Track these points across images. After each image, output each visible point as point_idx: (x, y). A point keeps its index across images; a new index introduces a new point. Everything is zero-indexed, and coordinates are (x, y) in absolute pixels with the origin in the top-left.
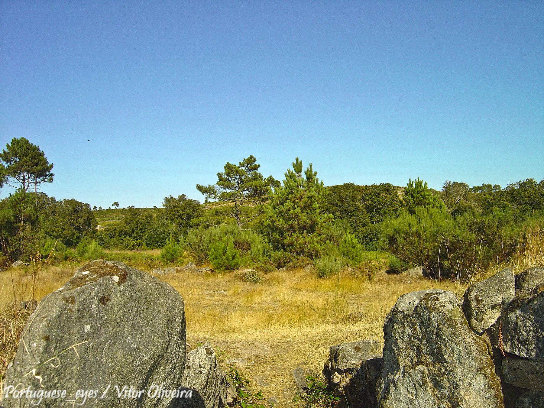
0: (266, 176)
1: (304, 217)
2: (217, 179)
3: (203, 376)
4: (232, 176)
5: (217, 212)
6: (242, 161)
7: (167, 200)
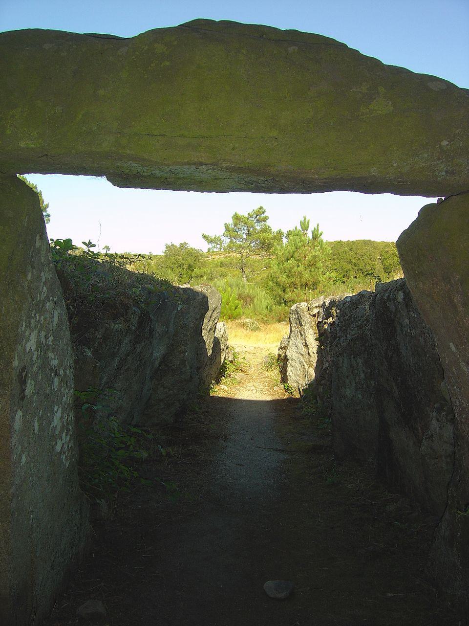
0: (275, 229)
1: (306, 275)
2: (224, 230)
3: (222, 333)
4: (239, 226)
5: (221, 263)
6: (250, 211)
7: (168, 247)
